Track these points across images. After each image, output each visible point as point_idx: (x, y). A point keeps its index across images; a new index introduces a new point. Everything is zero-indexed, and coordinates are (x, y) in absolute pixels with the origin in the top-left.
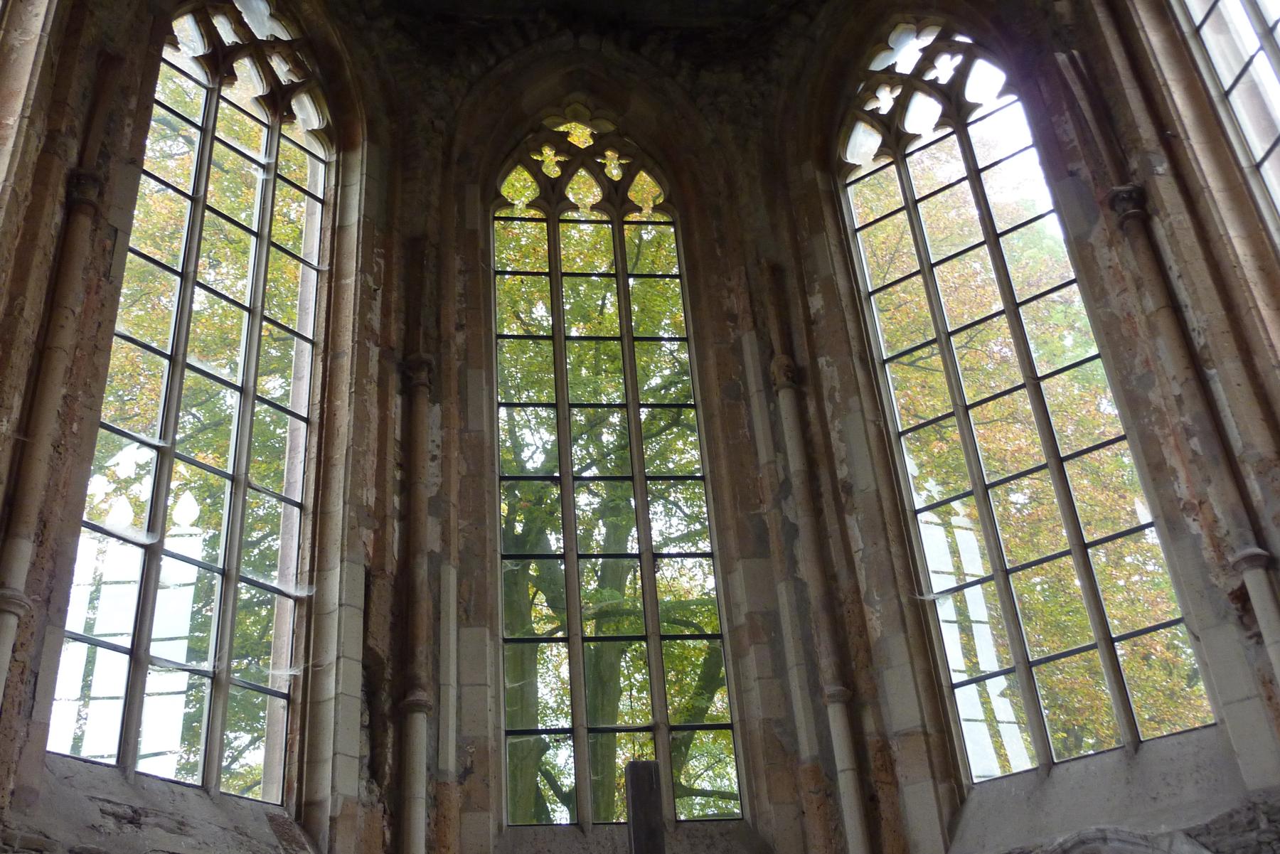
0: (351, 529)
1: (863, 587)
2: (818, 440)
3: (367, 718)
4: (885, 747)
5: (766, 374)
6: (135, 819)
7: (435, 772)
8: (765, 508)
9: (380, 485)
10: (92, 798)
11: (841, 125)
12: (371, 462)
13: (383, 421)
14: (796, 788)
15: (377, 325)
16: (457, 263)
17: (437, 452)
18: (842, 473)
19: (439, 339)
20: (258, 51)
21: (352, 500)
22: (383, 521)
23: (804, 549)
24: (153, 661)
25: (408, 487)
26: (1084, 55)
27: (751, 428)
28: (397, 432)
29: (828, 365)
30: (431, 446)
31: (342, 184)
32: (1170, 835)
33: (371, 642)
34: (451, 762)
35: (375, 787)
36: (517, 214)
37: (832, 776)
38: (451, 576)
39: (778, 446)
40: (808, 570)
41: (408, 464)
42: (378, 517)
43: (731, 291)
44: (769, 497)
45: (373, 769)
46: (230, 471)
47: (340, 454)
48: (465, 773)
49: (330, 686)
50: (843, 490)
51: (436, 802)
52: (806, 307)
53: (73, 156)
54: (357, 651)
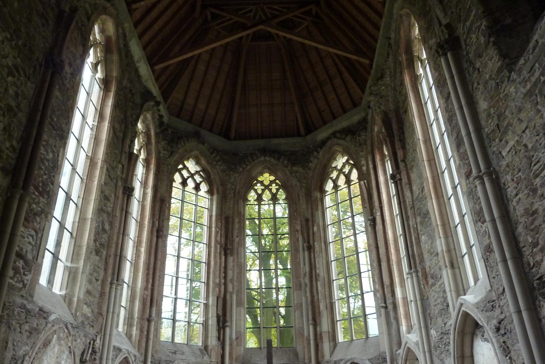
0: (214, 289)
4: (321, 334)
5: (303, 246)
7: (231, 338)
8: (302, 279)
9: (220, 278)
12: (218, 273)
14: (303, 342)
15: (219, 240)
16: (237, 220)
18: (318, 271)
19: (233, 241)
20: (192, 176)
21: (214, 282)
23: (308, 289)
24: (177, 321)
25: (225, 278)
26: (367, 182)
28: (223, 265)
31: (212, 204)
34: (234, 337)
36: (251, 203)
37: (310, 340)
38: (234, 297)
39: (305, 264)
40: (308, 294)
41: (225, 272)
42: (219, 285)
44: (302, 276)
45: (219, 338)
47: (211, 271)
48: (237, 338)
49: (210, 322)
50: (317, 275)
51: (231, 345)
52: (313, 229)
53: (157, 225)
54: (215, 315)
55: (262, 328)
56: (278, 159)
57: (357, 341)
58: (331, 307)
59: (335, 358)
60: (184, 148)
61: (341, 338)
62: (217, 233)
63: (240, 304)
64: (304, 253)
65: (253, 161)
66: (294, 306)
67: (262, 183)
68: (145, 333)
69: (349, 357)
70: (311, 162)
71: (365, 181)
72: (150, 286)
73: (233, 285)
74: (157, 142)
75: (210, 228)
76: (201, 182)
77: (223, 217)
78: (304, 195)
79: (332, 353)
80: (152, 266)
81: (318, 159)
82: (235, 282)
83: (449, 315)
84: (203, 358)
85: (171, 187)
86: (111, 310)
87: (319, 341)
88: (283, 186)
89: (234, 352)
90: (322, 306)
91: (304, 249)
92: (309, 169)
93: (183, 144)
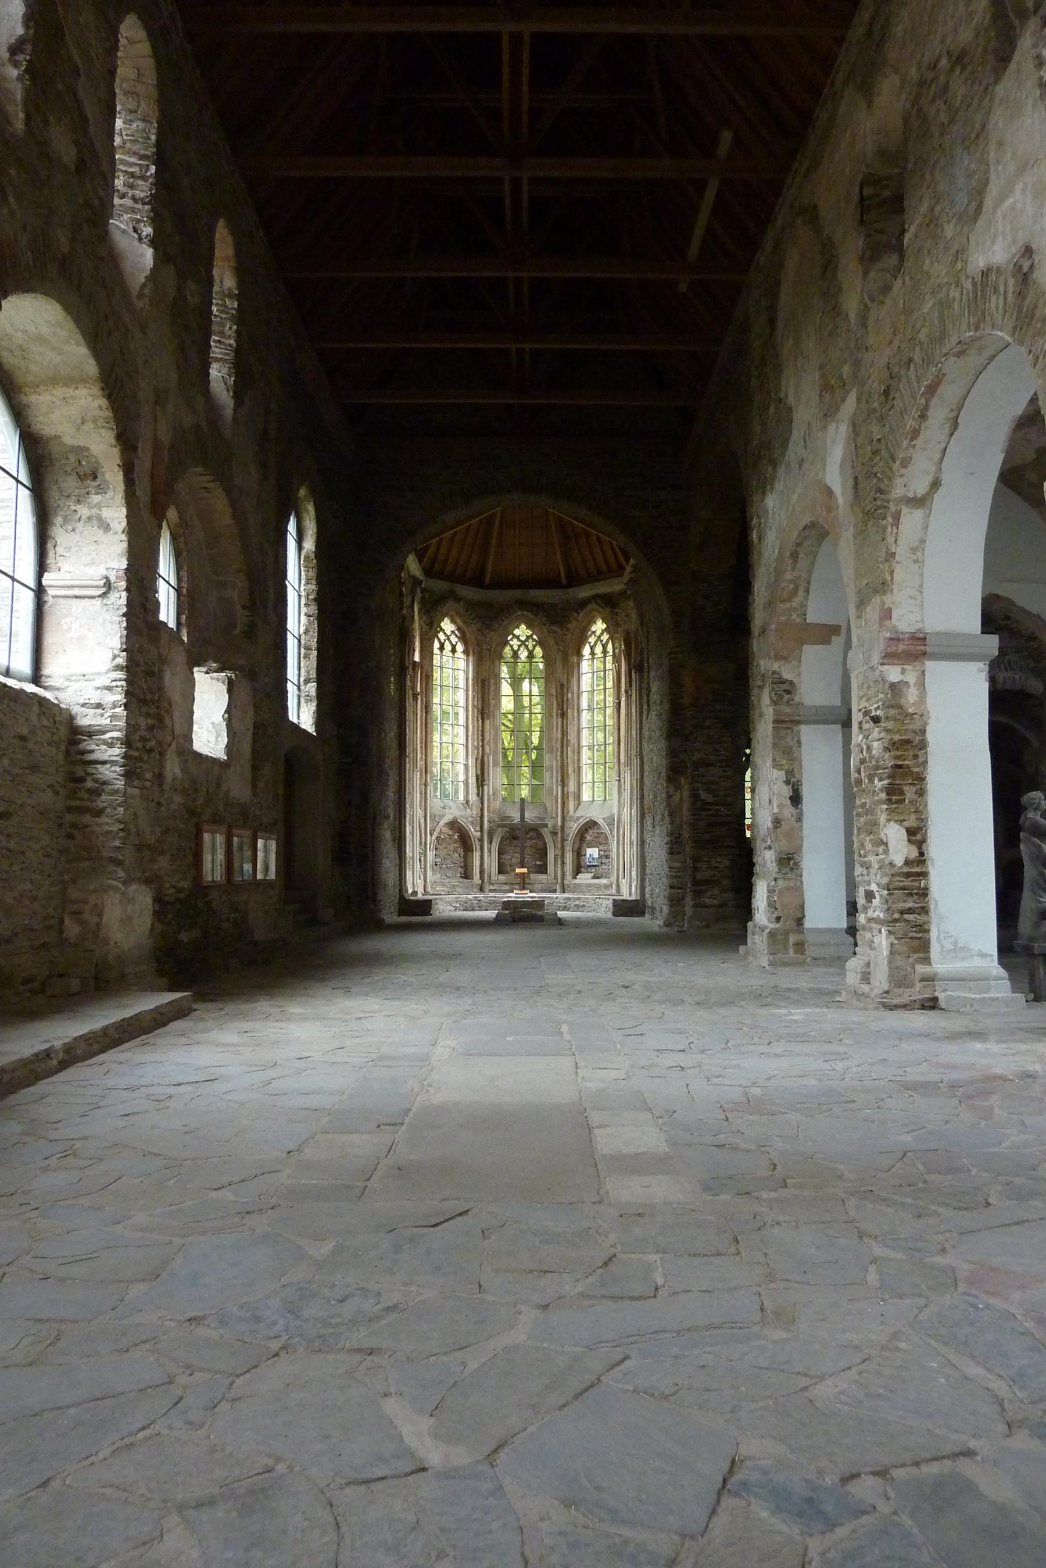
7: (488, 795)
21: (473, 745)
23: (559, 754)
25: (483, 740)
31: (468, 666)
40: (559, 758)
41: (482, 736)
47: (470, 734)
56: (536, 615)
58: (578, 771)
59: (578, 814)
62: (474, 696)
63: (496, 764)
67: (518, 637)
75: (467, 691)
79: (576, 810)
85: (432, 654)
88: (540, 643)
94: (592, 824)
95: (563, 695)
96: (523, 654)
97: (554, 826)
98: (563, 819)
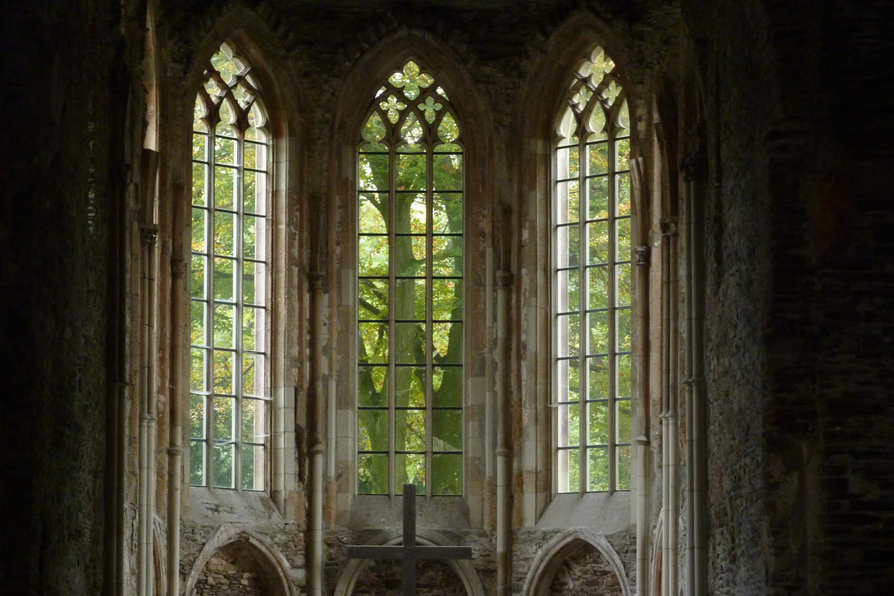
0: (288, 370)
1: (524, 399)
2: (514, 317)
3: (297, 455)
4: (520, 475)
5: (494, 275)
6: (216, 510)
8: (486, 350)
10: (203, 503)
11: (558, 108)
13: (301, 309)
14: (482, 489)
16: (337, 201)
17: (326, 321)
18: (523, 337)
22: (302, 363)
25: (313, 344)
26: (645, 162)
27: (485, 304)
28: (307, 315)
29: (526, 274)
30: (323, 318)
31: (276, 161)
32: (600, 535)
33: (298, 422)
34: (332, 473)
35: (301, 484)
37: (496, 486)
39: (495, 319)
40: (498, 388)
41: (313, 332)
42: (300, 361)
43: (484, 216)
44: (487, 345)
45: (300, 476)
46: (206, 160)
47: (282, 327)
48: (339, 476)
50: (522, 347)
51: (326, 490)
52: (520, 236)
54: (292, 428)
55: (392, 454)
57: (592, 495)
59: (545, 526)
60: (212, 31)
61: (564, 483)
62: (291, 237)
64: (495, 291)
65: (380, 38)
66: (467, 408)
67: (399, 92)
68: (166, 477)
69: (571, 529)
70: (528, 57)
71: (640, 159)
72: (167, 385)
73: (330, 359)
74: (160, 46)
75: (274, 223)
76: (250, 105)
77: (305, 195)
78: (502, 146)
79: (540, 515)
80: (168, 342)
81: (545, 52)
82: (334, 355)
83: (595, 554)
84: (270, 518)
86: (145, 465)
87: (515, 488)
89: (333, 504)
90: (527, 416)
91: (495, 283)
92: (521, 75)
93: (209, 23)
94: (579, 551)
95: (508, 234)
96: (413, 134)
97: (488, 554)
98: (510, 536)
